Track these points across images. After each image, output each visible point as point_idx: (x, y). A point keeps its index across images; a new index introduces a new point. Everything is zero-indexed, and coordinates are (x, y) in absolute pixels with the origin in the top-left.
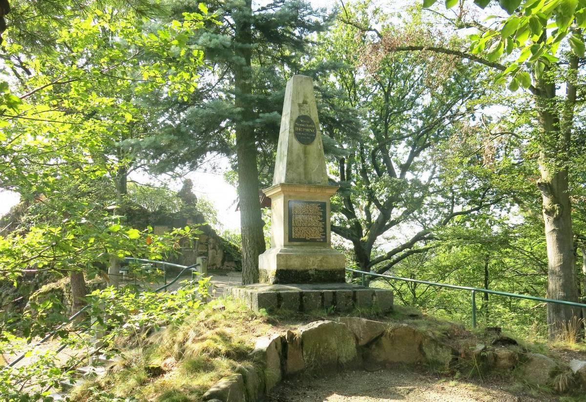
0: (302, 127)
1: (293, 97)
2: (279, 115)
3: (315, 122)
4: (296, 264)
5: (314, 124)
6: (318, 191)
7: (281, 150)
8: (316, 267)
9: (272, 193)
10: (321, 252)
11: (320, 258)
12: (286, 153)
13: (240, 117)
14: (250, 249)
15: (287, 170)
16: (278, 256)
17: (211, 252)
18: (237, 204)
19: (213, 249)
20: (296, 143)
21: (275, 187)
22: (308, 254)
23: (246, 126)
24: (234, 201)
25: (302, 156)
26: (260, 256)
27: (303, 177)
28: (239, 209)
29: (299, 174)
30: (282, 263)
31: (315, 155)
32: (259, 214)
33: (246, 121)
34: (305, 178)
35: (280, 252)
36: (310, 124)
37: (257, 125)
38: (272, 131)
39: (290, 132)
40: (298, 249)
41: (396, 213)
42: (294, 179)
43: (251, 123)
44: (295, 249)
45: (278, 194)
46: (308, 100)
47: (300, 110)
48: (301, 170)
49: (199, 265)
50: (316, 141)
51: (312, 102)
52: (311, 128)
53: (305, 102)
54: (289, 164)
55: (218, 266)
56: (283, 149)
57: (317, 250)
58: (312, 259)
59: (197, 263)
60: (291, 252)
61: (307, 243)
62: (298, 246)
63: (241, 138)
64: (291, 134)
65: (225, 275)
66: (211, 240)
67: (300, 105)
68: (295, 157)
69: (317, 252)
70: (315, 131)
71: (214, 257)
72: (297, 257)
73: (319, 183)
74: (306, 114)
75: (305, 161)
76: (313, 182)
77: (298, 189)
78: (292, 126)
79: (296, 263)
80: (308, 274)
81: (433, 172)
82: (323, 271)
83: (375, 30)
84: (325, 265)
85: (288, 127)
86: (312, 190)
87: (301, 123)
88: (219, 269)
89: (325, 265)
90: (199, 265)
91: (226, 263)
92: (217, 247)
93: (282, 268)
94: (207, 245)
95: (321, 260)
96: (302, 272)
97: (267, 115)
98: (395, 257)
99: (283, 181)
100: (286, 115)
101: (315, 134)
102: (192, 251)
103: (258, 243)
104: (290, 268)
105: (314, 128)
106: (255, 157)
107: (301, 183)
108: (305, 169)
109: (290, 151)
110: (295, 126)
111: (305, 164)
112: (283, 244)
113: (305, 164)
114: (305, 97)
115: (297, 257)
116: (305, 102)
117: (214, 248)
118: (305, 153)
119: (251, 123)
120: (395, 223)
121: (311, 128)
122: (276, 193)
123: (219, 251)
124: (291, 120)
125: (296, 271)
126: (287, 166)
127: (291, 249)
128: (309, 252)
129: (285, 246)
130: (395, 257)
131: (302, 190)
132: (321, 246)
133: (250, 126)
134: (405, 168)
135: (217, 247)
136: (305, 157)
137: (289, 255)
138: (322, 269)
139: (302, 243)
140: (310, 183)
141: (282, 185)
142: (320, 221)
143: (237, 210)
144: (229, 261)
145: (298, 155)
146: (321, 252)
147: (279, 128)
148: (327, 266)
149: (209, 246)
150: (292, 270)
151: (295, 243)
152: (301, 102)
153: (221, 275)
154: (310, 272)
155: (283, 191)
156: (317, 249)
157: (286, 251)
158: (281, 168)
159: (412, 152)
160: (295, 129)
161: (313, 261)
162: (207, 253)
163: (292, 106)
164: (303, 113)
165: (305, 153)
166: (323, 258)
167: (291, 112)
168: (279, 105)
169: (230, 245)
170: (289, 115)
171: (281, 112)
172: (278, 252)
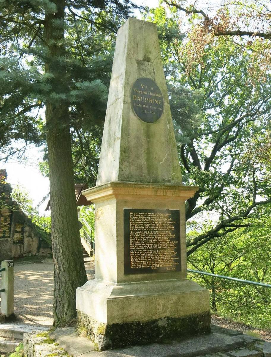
0: (142, 95)
1: (129, 49)
2: (103, 87)
3: (161, 89)
4: (138, 312)
5: (160, 92)
6: (169, 194)
7: (110, 129)
8: (168, 314)
9: (97, 196)
10: (174, 288)
11: (174, 299)
12: (119, 135)
13: (47, 87)
14: (63, 261)
15: (122, 161)
16: (110, 302)
17: (26, 240)
18: (48, 200)
19: (28, 236)
20: (134, 120)
21: (102, 188)
22: (156, 294)
23: (57, 100)
24: (44, 199)
25: (143, 138)
26: (79, 291)
27: (145, 171)
28: (50, 208)
29: (140, 168)
30: (115, 313)
31: (163, 139)
32: (75, 213)
33: (58, 93)
34: (149, 174)
35: (113, 293)
36: (153, 92)
37: (73, 99)
38: (94, 110)
39: (125, 102)
40: (143, 287)
41: (200, 202)
42: (132, 175)
43: (64, 96)
44: (135, 286)
45: (107, 198)
46: (152, 57)
47: (139, 69)
48: (143, 161)
49: (4, 269)
50: (163, 117)
51: (157, 60)
52: (155, 98)
53: (147, 59)
54: (125, 152)
55: (34, 253)
56: (113, 128)
57: (169, 285)
58: (162, 302)
59: (2, 268)
60: (130, 292)
61: (153, 274)
62: (138, 280)
63: (52, 119)
64: (126, 106)
65: (41, 263)
66: (27, 229)
67: (139, 62)
68: (133, 143)
69: (168, 288)
70: (162, 103)
71: (29, 245)
72: (141, 300)
73: (169, 181)
74: (149, 77)
75: (148, 149)
76: (160, 179)
77: (139, 192)
78: (128, 94)
79: (138, 310)
80: (157, 326)
81: (232, 165)
82: (178, 319)
83: (201, 12)
84: (182, 309)
85: (121, 94)
86: (160, 193)
87: (140, 89)
88: (35, 255)
89: (182, 309)
90: (4, 269)
91: (42, 250)
92: (33, 235)
93: (116, 321)
94: (23, 234)
95: (176, 303)
96: (148, 324)
97: (86, 84)
98: (198, 243)
99: (114, 176)
100: (117, 78)
101: (162, 107)
102: (7, 240)
103: (73, 253)
104: (129, 320)
105: (161, 98)
106: (70, 147)
107: (142, 182)
108: (148, 159)
109: (125, 131)
110: (133, 93)
111: (149, 153)
112: (115, 278)
113: (149, 153)
114: (147, 51)
115: (141, 300)
116: (147, 59)
117: (30, 236)
118: (149, 135)
119: (64, 96)
120: (199, 210)
121: (155, 98)
122: (104, 197)
123: (34, 239)
124: (127, 83)
125: (138, 324)
126: (121, 155)
127: (128, 287)
128: (158, 291)
129: (119, 282)
130: (198, 243)
131: (145, 192)
132: (172, 277)
133: (62, 100)
134: (209, 161)
135: (33, 235)
136: (148, 142)
137: (128, 299)
138: (177, 316)
139: (146, 275)
140: (155, 181)
141: (114, 185)
142: (171, 239)
143: (47, 209)
144: (45, 248)
145: (138, 138)
146: (174, 288)
147: (104, 105)
148: (184, 312)
149: (24, 234)
150: (132, 323)
151: (136, 276)
152: (141, 58)
153: (37, 262)
154: (160, 324)
155: (116, 195)
156: (168, 283)
157: (121, 292)
158: (110, 156)
159: (215, 147)
160: (132, 98)
161: (164, 305)
162: (23, 241)
163: (127, 62)
164: (144, 75)
165: (149, 135)
166: (179, 299)
167: (126, 71)
168: (104, 71)
169: (46, 232)
170: (124, 76)
171: (107, 81)
172: (109, 295)
